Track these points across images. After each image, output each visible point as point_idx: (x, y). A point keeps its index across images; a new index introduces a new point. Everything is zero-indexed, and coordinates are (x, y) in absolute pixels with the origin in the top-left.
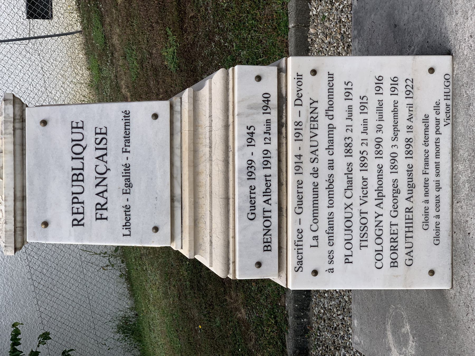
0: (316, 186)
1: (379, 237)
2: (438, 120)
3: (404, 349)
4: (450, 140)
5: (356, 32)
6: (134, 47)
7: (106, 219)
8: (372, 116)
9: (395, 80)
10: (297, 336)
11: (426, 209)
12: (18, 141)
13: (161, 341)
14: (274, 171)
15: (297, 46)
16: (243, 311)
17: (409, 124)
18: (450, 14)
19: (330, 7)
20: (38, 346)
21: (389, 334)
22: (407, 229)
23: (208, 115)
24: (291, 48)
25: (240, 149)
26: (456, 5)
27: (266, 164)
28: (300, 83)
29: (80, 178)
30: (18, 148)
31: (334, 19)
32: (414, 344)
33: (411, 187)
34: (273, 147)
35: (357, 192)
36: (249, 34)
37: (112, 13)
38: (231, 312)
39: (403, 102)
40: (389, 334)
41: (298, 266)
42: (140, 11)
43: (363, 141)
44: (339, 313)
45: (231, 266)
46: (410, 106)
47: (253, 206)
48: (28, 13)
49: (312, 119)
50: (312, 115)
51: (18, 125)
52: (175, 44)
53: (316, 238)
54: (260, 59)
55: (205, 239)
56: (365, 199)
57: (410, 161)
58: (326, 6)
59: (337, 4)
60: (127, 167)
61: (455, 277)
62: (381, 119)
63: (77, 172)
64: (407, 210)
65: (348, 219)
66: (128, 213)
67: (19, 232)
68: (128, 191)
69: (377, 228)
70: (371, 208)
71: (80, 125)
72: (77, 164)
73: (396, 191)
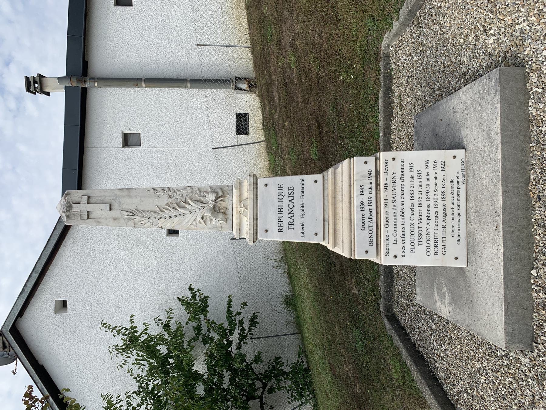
0: (395, 214)
1: (428, 240)
2: (458, 182)
3: (443, 301)
4: (465, 192)
5: (416, 138)
6: (294, 148)
7: (293, 229)
8: (424, 180)
9: (435, 162)
10: (386, 301)
11: (453, 226)
12: (255, 193)
13: (308, 307)
14: (374, 207)
15: (384, 145)
16: (355, 289)
17: (444, 184)
18: (464, 129)
19: (402, 124)
20: (241, 309)
21: (436, 293)
22: (443, 236)
23: (341, 181)
24: (381, 146)
25: (357, 196)
26: (466, 125)
27: (370, 203)
28: (387, 165)
29: (282, 210)
30: (255, 196)
31: (404, 131)
32: (449, 297)
33: (445, 215)
34: (373, 195)
35: (417, 217)
36: (358, 139)
37: (282, 131)
38: (348, 290)
39: (440, 173)
40: (436, 293)
41: (387, 253)
42: (298, 129)
43: (420, 192)
44: (409, 287)
45: (353, 252)
46: (444, 175)
47: (363, 223)
48: (237, 132)
49: (393, 182)
50: (393, 180)
51: (255, 186)
52: (316, 146)
53: (395, 240)
54: (364, 153)
55: (340, 239)
56: (421, 221)
57: (444, 202)
58: (400, 124)
59: (406, 123)
60: (303, 205)
61: (469, 261)
62: (428, 181)
63: (280, 207)
64: (443, 227)
65: (412, 231)
66: (303, 227)
67: (255, 234)
68: (303, 216)
69: (427, 235)
70: (424, 225)
71: (282, 186)
72: (280, 204)
73: (437, 217)
